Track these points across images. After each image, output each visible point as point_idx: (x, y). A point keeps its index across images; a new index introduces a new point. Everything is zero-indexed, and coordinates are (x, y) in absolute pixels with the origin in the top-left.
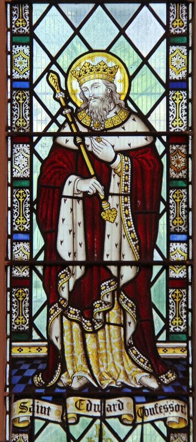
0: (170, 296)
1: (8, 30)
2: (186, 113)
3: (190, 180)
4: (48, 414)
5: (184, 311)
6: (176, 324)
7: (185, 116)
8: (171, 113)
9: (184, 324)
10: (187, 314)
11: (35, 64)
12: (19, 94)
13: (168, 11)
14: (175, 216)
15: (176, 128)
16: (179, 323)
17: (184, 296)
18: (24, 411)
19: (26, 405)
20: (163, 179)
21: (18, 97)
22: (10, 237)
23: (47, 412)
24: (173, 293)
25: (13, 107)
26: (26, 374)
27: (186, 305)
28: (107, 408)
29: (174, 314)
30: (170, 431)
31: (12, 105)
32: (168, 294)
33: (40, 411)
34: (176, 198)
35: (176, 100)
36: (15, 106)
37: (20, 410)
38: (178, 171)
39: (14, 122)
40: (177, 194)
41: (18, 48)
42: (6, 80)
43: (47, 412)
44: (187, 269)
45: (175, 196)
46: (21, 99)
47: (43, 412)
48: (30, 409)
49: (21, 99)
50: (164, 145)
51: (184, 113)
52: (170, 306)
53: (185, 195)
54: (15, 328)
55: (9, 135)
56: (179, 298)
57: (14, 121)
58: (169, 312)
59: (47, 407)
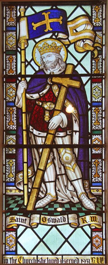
0: (93, 10)
1: (4, 99)
2: (101, 171)
3: (104, 44)
4: (25, 223)
5: (100, 118)
6: (96, 21)
7: (101, 68)
8: (93, 119)
9: (100, 177)
10: (102, 120)
11: (21, 248)
12: (10, 161)
13: (92, 8)
14: (95, 121)
15: (95, 178)
16: (98, 21)
17: (100, 111)
18: (13, 221)
19: (14, 218)
20: (90, 115)
21: (9, 163)
22: (5, 52)
23: (24, 222)
24: (94, 162)
25: (7, 168)
26: (11, 207)
27: (101, 168)
28: (57, 221)
29: (95, 172)
30: (92, 230)
31: (6, 167)
32: (92, 63)
33: (20, 221)
34: (96, 164)
35: (96, 112)
36: (7, 167)
37: (10, 221)
38: (97, 248)
39: (7, 123)
40: (96, 110)
41: (10, 33)
42: (2, 215)
43: (24, 222)
44: (103, 6)
45: (95, 111)
46: (11, 164)
47: (22, 221)
48: (16, 220)
49: (11, 164)
50: (90, 239)
51: (101, 66)
52: (93, 64)
53: (101, 110)
54: (8, 128)
55: (5, 77)
56: (98, 164)
57: (7, 175)
58: (92, 171)
59: (24, 219)
